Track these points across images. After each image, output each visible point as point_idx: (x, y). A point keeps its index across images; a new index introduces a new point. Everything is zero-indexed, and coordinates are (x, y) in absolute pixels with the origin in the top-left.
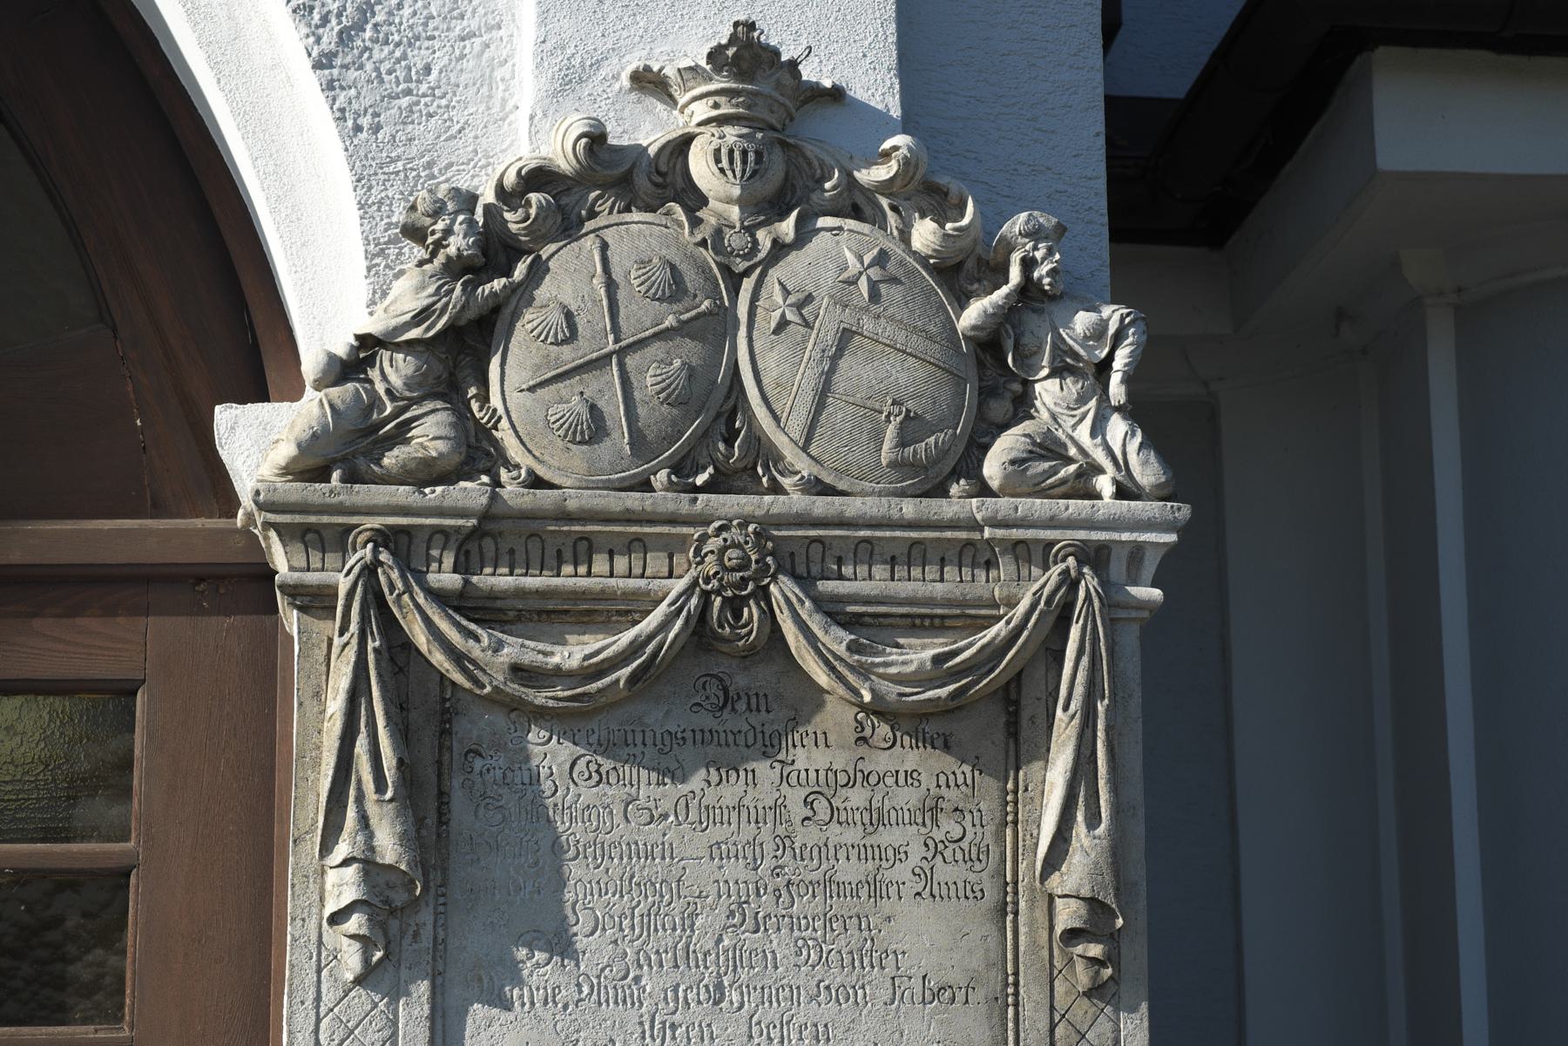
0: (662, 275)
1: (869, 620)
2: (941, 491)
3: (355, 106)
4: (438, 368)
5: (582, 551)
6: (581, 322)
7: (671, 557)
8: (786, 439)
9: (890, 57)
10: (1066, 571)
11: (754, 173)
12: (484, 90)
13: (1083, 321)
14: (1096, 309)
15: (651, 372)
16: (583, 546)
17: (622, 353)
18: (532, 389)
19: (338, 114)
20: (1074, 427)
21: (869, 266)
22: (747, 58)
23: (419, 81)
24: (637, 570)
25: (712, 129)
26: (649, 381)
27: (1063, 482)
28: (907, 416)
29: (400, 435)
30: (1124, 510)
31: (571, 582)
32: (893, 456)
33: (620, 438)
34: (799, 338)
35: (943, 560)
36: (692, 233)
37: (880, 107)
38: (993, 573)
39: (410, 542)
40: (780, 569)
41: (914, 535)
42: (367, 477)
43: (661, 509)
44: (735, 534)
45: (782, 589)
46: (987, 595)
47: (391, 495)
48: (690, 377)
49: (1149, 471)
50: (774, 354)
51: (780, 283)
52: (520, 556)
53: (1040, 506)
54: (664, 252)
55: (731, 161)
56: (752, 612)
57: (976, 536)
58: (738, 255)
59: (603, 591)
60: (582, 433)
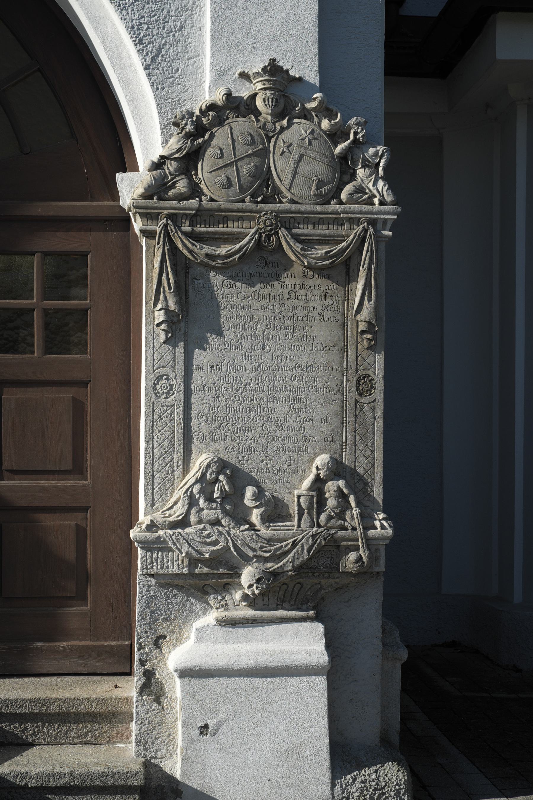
0: (248, 137)
1: (307, 241)
2: (328, 203)
3: (157, 81)
5: (225, 220)
6: (225, 152)
7: (250, 222)
12: (195, 76)
13: (371, 151)
15: (245, 167)
17: (236, 161)
18: (211, 172)
20: (368, 183)
22: (273, 70)
23: (175, 73)
24: (241, 226)
27: (364, 200)
29: (173, 186)
31: (222, 229)
33: (236, 187)
36: (257, 124)
41: (320, 216)
43: (248, 208)
44: (269, 216)
45: (282, 232)
53: (357, 207)
54: (249, 130)
57: (338, 216)
59: (231, 232)
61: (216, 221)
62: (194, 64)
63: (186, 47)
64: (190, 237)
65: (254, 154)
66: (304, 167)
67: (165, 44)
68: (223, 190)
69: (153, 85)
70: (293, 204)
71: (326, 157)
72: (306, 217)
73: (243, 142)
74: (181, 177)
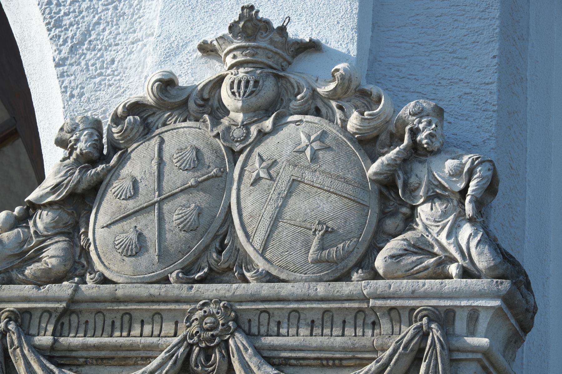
0: (190, 155)
1: (293, 362)
2: (346, 277)
3: (73, 84)
4: (66, 218)
5: (127, 321)
6: (141, 186)
7: (176, 323)
8: (252, 249)
9: (353, 22)
10: (421, 327)
11: (252, 92)
12: (140, 69)
13: (450, 164)
14: (458, 157)
15: (177, 212)
16: (126, 318)
17: (159, 202)
18: (108, 226)
19: (63, 90)
20: (439, 233)
21: (313, 141)
22: (250, 26)
23: (107, 68)
24: (156, 333)
25: (234, 71)
26: (175, 217)
27: (426, 268)
28: (326, 231)
29: (36, 257)
30: (463, 285)
31: (121, 340)
32: (315, 256)
33: (153, 253)
34: (266, 187)
35: (344, 322)
36: (212, 130)
37: (344, 51)
38: (377, 331)
39: (31, 318)
40: (239, 328)
41: (325, 306)
42: (17, 281)
43: (170, 294)
44: (212, 308)
45: (238, 341)
46: (368, 344)
47: (21, 290)
48: (199, 214)
49: (483, 258)
50: (251, 198)
51: (259, 155)
52: (91, 325)
53: (406, 285)
54: (195, 143)
55: (239, 88)
56: (216, 356)
57: (365, 305)
58: (237, 141)
59: (131, 345)
60: (132, 250)
61: (108, 322)
62: (142, 49)
63: (132, 24)
64: (44, 356)
65: (197, 186)
66: (299, 206)
67: (98, 23)
68: (125, 258)
69: (66, 92)
70: (269, 281)
71: (347, 182)
72: (295, 310)
73: (178, 164)
74: (57, 239)
